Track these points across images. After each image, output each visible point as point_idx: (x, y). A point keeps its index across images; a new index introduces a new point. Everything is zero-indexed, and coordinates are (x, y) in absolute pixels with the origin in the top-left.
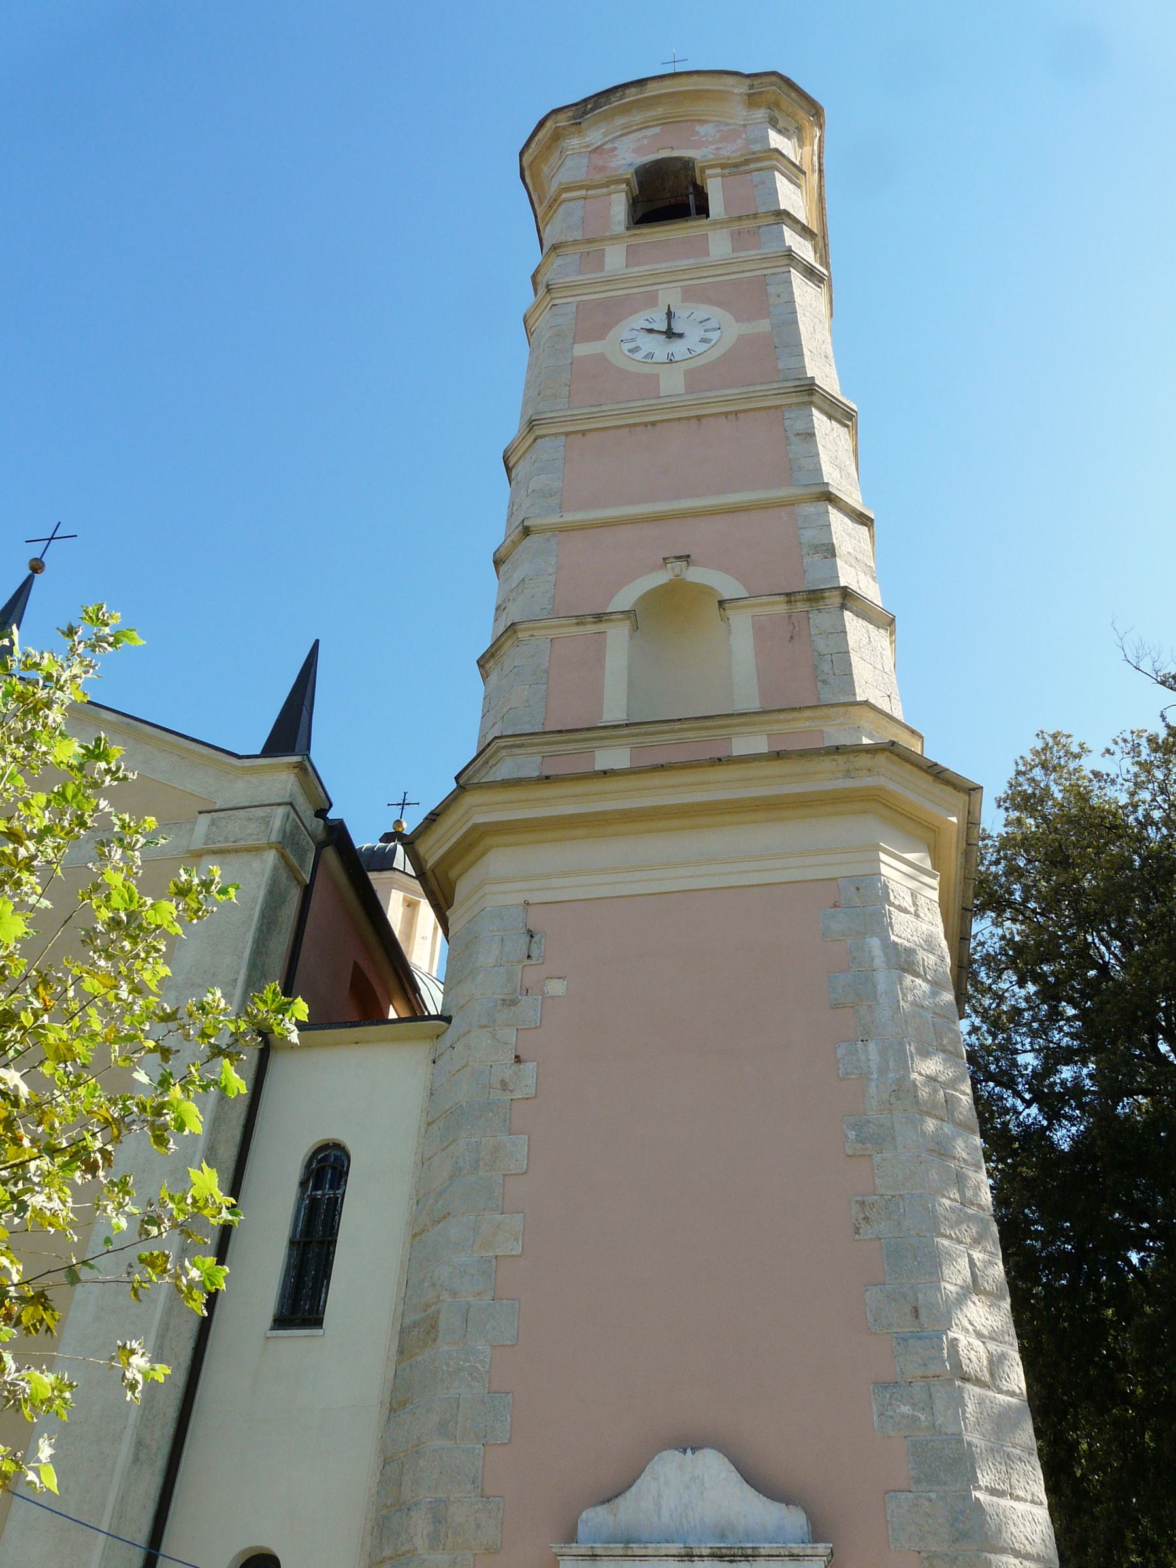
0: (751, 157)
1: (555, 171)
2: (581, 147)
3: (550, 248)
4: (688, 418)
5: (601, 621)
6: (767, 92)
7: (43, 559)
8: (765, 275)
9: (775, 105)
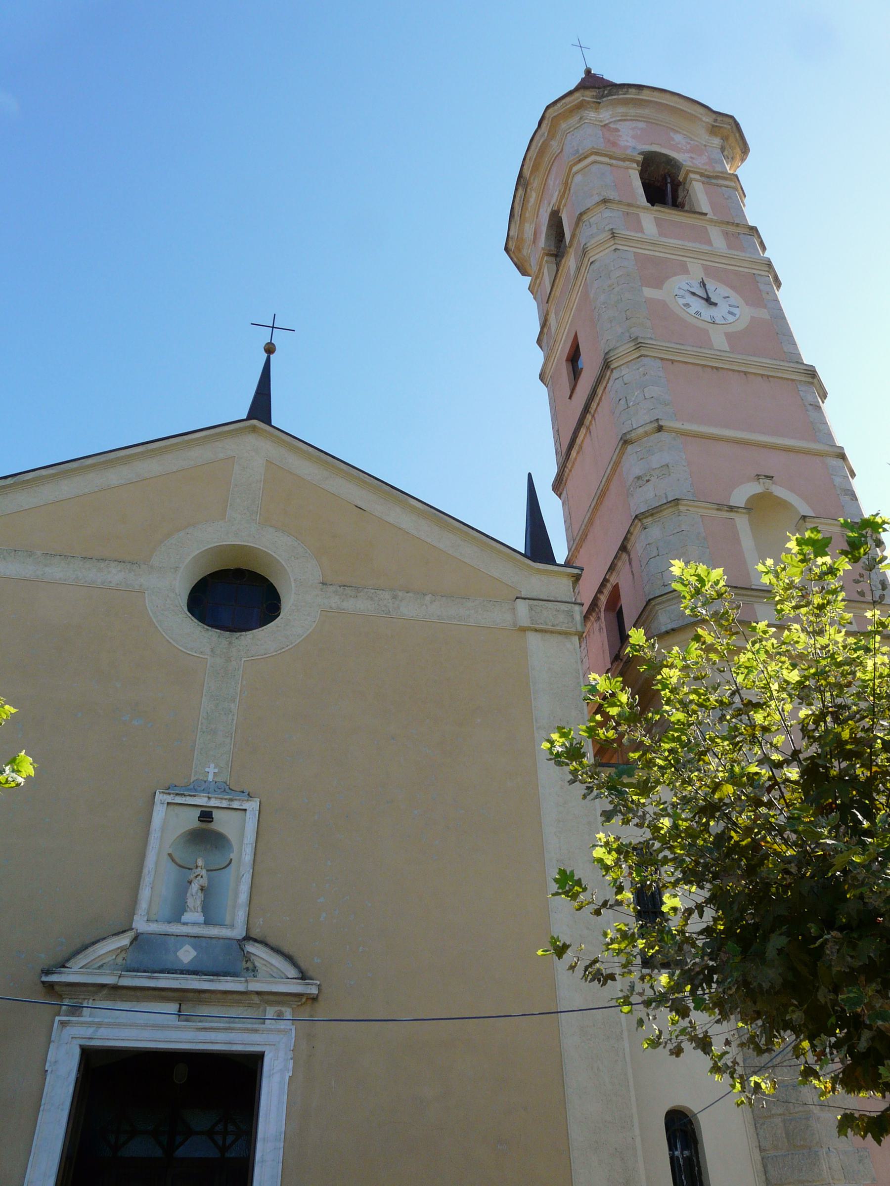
0: (721, 175)
1: (572, 129)
2: (596, 120)
3: (602, 200)
4: (739, 371)
5: (732, 511)
6: (725, 128)
7: (272, 342)
8: (754, 274)
9: (725, 138)
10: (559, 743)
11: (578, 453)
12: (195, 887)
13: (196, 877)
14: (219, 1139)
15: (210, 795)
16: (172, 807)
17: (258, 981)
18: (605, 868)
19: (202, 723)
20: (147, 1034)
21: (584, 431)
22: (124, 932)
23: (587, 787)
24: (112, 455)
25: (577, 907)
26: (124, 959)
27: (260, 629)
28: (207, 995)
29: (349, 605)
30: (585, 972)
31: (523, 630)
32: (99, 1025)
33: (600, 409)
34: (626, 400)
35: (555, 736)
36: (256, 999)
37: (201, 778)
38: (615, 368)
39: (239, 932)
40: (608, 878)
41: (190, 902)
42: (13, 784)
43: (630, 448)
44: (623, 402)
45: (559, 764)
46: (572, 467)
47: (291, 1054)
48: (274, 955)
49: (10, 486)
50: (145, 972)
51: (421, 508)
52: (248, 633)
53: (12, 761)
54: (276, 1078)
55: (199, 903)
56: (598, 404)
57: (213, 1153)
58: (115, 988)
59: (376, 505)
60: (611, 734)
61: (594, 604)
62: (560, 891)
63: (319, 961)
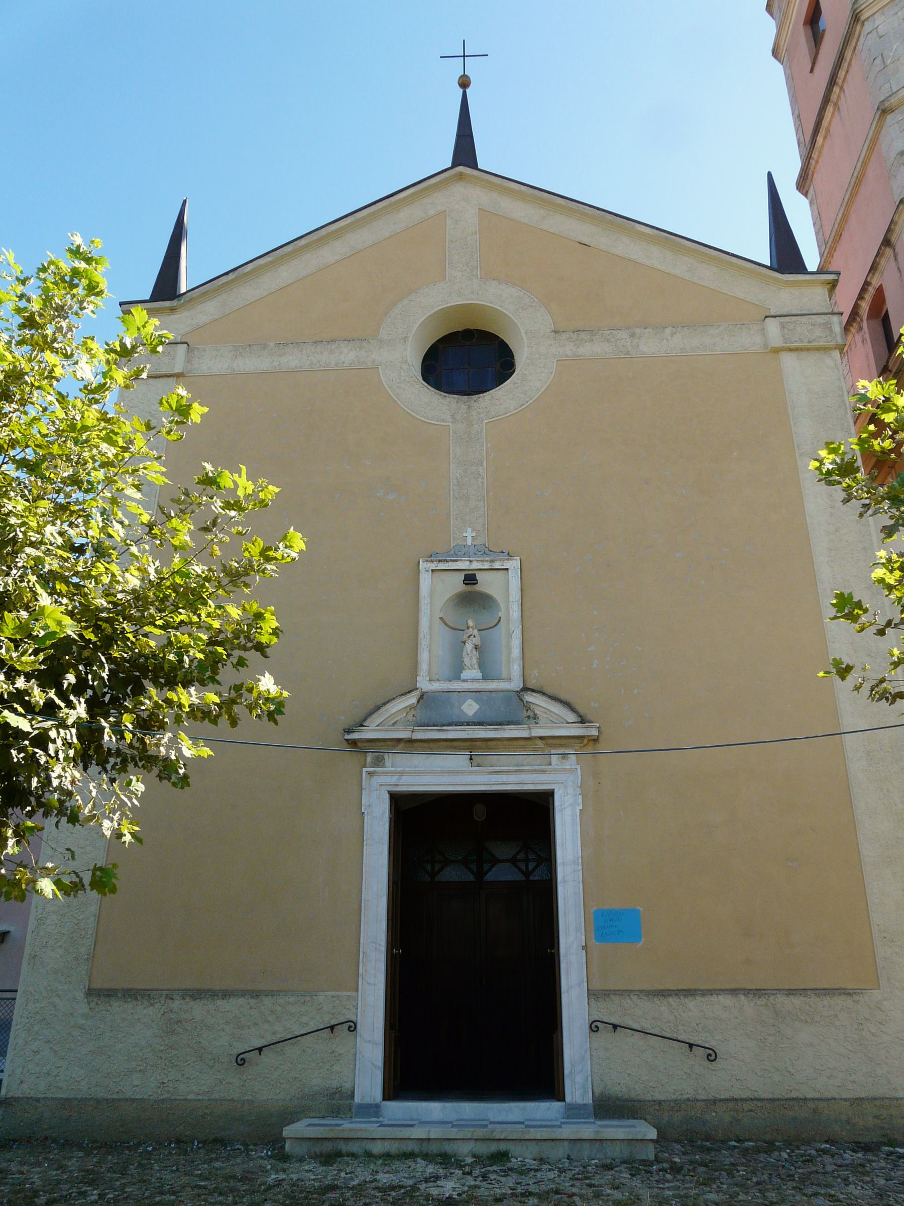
10: (829, 461)
11: (825, 138)
12: (469, 646)
13: (469, 637)
14: (522, 866)
15: (471, 559)
16: (437, 574)
17: (540, 727)
18: (887, 588)
19: (453, 490)
20: (445, 779)
21: (831, 110)
22: (410, 692)
23: (863, 505)
24: (324, 231)
25: (859, 629)
26: (414, 716)
27: (497, 388)
28: (494, 743)
29: (585, 350)
30: (872, 691)
31: (776, 351)
32: (402, 773)
33: (849, 77)
34: (883, 58)
35: (823, 453)
36: (540, 744)
37: (461, 543)
38: (866, 20)
39: (516, 684)
40: (891, 596)
41: (467, 661)
42: (289, 560)
43: (889, 118)
44: (878, 61)
45: (830, 483)
46: (818, 157)
47: (578, 791)
48: (553, 702)
49: (232, 281)
50: (434, 726)
51: (650, 233)
52: (485, 394)
53: (284, 538)
54: (568, 813)
55: (475, 661)
56: (847, 71)
57: (520, 877)
58: (410, 741)
59: (600, 238)
60: (888, 444)
61: (855, 313)
62: (839, 615)
63: (597, 705)
